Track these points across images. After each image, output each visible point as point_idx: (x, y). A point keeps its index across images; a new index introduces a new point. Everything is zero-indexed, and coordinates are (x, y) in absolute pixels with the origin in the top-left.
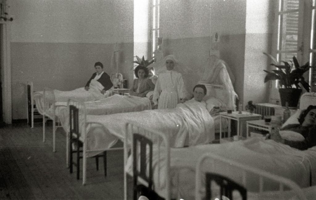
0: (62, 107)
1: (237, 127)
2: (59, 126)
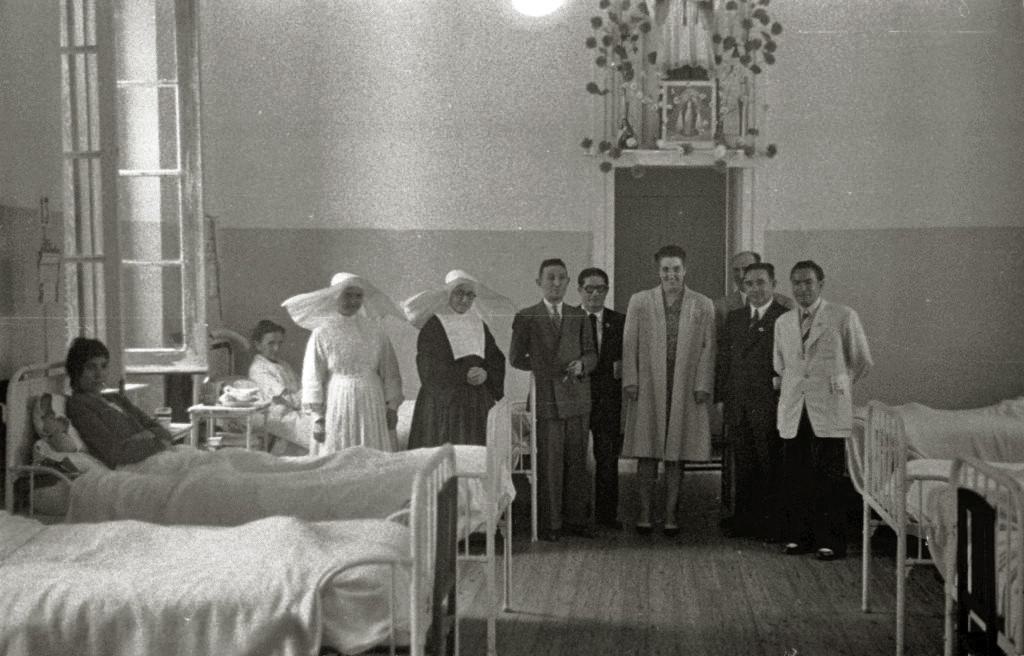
0: (928, 486)
1: (868, 567)
2: (920, 560)
